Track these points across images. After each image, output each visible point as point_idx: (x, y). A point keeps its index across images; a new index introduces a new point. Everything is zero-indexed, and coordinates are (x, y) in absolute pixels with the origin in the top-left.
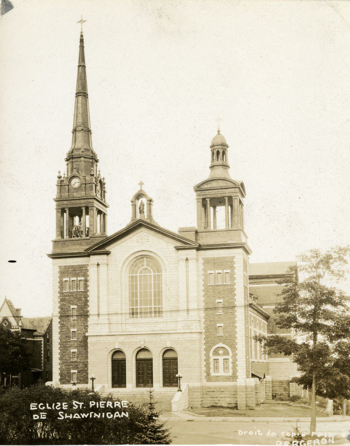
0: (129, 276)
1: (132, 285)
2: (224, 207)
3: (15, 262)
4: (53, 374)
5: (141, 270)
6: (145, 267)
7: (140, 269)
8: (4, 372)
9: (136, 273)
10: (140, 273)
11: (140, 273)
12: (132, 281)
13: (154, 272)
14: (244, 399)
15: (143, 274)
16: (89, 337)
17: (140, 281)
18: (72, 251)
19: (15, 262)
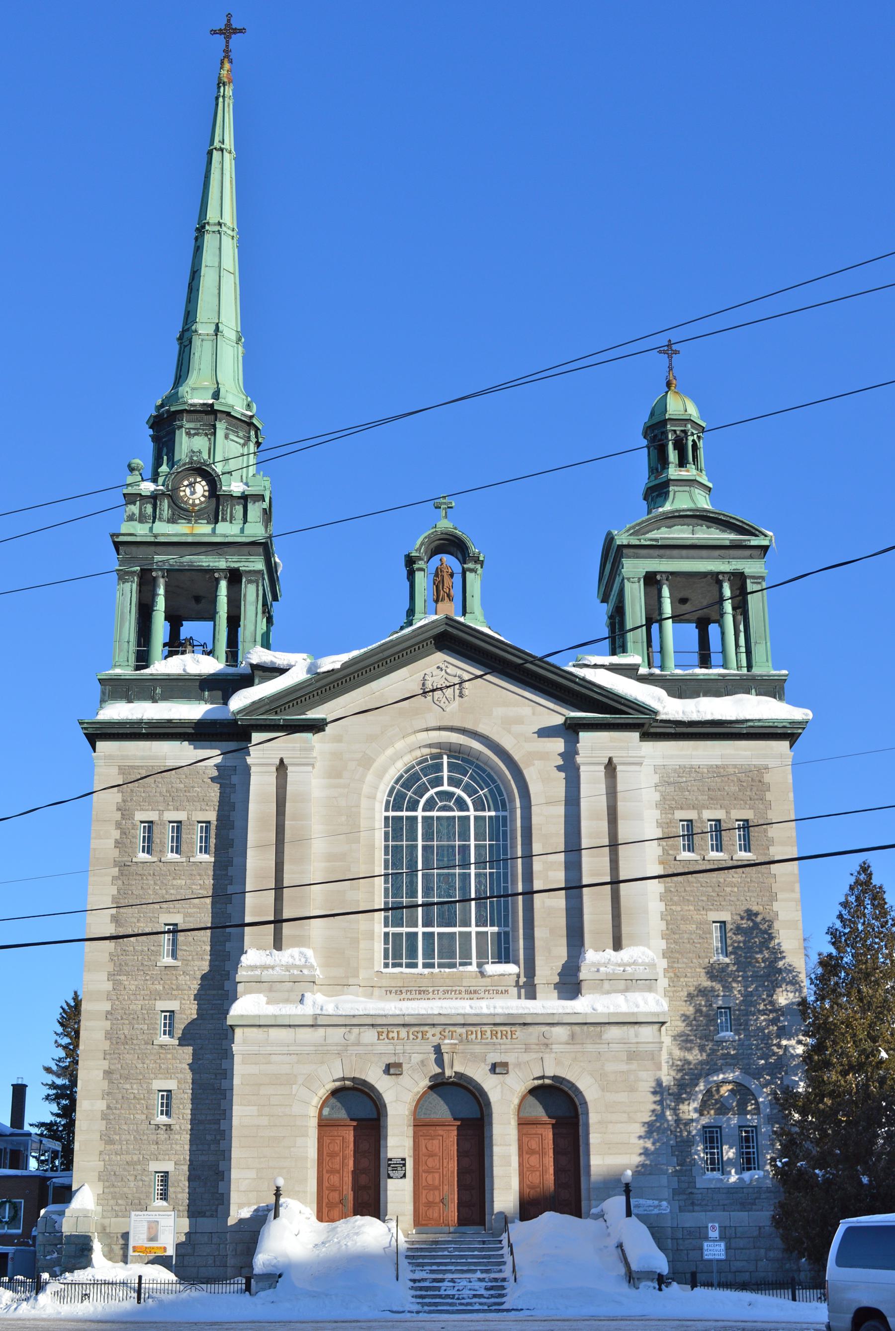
0: (387, 818)
1: (397, 850)
2: (606, 604)
3: (397, 1280)
4: (494, 1115)
5: (432, 797)
6: (446, 787)
7: (427, 796)
8: (837, 1154)
9: (413, 806)
10: (424, 810)
11: (424, 810)
12: (397, 836)
13: (479, 805)
14: (278, 962)
15: (435, 814)
16: (238, 1032)
17: (427, 836)
18: (477, 625)
19: (397, 1280)
